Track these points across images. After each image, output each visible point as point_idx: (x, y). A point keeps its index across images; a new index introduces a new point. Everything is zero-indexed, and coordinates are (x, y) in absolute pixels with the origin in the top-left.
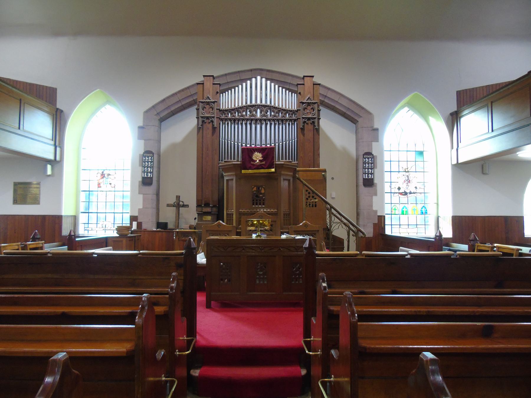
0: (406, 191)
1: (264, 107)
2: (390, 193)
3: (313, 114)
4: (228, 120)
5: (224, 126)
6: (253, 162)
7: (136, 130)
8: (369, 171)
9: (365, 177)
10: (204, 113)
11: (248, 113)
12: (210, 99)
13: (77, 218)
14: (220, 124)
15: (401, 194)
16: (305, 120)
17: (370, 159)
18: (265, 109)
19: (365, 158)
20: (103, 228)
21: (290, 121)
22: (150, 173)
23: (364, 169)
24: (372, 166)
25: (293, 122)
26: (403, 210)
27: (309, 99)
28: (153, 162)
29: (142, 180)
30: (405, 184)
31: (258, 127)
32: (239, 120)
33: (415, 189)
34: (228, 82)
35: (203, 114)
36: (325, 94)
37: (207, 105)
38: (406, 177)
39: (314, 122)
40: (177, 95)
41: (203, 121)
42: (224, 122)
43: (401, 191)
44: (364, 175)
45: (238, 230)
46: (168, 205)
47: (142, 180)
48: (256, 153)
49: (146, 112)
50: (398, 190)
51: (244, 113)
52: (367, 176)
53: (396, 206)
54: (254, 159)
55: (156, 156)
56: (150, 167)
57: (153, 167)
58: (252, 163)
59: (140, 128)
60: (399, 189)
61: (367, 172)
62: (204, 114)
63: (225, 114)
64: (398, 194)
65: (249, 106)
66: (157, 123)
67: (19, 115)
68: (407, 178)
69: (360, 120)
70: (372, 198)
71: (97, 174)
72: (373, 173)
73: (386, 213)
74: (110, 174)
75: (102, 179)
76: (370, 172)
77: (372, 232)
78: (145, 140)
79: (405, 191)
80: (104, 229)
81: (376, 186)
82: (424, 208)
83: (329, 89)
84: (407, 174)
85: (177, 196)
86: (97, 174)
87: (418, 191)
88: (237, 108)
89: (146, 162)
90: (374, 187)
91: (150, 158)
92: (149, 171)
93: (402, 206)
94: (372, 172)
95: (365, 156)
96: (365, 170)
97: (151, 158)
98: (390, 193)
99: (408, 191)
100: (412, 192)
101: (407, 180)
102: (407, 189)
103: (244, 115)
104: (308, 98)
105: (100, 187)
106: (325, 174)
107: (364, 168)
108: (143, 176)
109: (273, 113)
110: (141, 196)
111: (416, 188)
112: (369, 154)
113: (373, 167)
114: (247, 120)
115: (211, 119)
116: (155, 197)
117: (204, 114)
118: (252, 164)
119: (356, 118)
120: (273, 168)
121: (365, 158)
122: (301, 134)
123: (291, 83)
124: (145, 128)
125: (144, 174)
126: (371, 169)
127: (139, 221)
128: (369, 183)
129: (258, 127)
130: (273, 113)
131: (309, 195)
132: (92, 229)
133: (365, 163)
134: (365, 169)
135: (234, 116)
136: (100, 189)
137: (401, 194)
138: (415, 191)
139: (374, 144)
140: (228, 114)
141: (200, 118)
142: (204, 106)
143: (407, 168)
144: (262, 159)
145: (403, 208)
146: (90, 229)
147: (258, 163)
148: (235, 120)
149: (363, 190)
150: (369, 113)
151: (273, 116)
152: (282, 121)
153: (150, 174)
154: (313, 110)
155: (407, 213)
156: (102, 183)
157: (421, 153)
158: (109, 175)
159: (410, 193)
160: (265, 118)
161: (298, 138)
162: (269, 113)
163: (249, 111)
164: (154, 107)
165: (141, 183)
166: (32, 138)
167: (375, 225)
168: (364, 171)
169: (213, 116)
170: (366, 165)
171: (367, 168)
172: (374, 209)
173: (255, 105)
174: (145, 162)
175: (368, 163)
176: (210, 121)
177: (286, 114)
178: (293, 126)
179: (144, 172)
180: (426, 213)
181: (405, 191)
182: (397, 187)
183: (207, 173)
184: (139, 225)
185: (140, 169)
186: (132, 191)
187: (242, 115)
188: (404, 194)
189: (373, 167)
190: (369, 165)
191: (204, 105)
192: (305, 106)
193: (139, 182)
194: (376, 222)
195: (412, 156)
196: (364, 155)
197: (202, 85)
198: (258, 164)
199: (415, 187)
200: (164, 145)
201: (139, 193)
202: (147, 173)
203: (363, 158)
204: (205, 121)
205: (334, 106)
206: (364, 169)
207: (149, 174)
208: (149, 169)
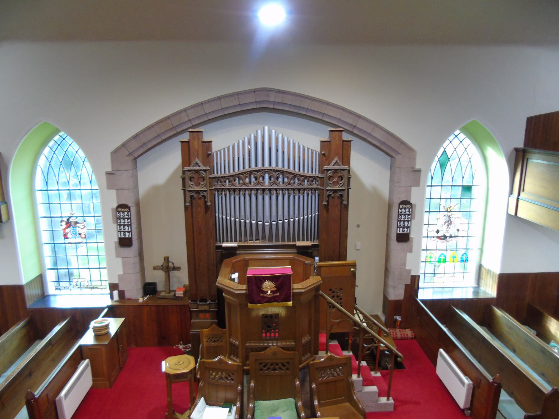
0: (446, 234)
1: (274, 173)
3: (341, 184)
4: (226, 190)
5: (220, 197)
6: (262, 293)
7: (104, 177)
8: (405, 224)
9: (400, 231)
10: (192, 185)
11: (253, 180)
12: (199, 166)
13: (43, 276)
14: (215, 195)
15: (439, 238)
16: (330, 193)
17: (407, 210)
18: (275, 175)
19: (401, 209)
20: (77, 287)
21: (309, 190)
22: (128, 232)
23: (399, 222)
24: (409, 218)
25: (313, 192)
26: (440, 257)
27: (336, 164)
28: (130, 218)
30: (445, 226)
31: (267, 198)
32: (240, 190)
33: (457, 231)
34: (223, 108)
35: (190, 187)
36: (354, 124)
37: (196, 173)
38: (447, 217)
39: (341, 196)
40: (154, 127)
41: (192, 197)
42: (220, 192)
43: (439, 235)
44: (398, 229)
45: (245, 368)
46: (155, 268)
47: (118, 240)
48: (267, 282)
49: (115, 153)
50: (436, 233)
51: (247, 180)
52: (403, 230)
53: (432, 253)
54: (264, 290)
55: (133, 210)
56: (128, 225)
57: (131, 225)
58: (262, 295)
59: (108, 173)
60: (438, 232)
62: (192, 186)
63: (221, 182)
64: (435, 238)
65: (253, 171)
66: (130, 165)
68: (448, 218)
69: (398, 157)
70: (406, 256)
71: (61, 222)
72: (409, 227)
73: (420, 273)
74: (78, 221)
75: (69, 229)
76: (406, 225)
77: (403, 294)
78: (116, 189)
79: (444, 234)
80: (79, 288)
81: (412, 242)
82: (465, 255)
83: (360, 117)
84: (449, 214)
85: (165, 258)
86: (61, 222)
87: (460, 234)
88: (238, 173)
89: (122, 219)
90: (409, 243)
91: (407, 210)
92: (127, 230)
93: (439, 253)
94: (409, 226)
95: (401, 206)
97: (128, 213)
99: (448, 235)
100: (453, 236)
101: (448, 221)
102: (447, 232)
103: (247, 183)
104: (335, 162)
105: (67, 238)
106: (354, 270)
107: (399, 221)
108: (120, 236)
109: (286, 180)
110: (120, 260)
111: (458, 230)
112: (406, 203)
113: (410, 219)
114: (251, 190)
115: (203, 193)
116: (137, 260)
117: (192, 186)
118: (262, 296)
119: (393, 154)
120: (291, 301)
121: (401, 209)
122: (324, 210)
123: (309, 108)
124: (116, 174)
125: (120, 233)
126: (408, 221)
127: (120, 289)
128: (404, 238)
129: (267, 198)
130: (286, 180)
131: (336, 296)
132: (64, 288)
133: (400, 214)
134: (401, 221)
135: (233, 185)
136: (67, 241)
137: (439, 238)
138: (456, 235)
139: (414, 189)
140: (225, 182)
141: (187, 193)
142: (191, 175)
143: (449, 207)
144: (275, 289)
145: (441, 256)
146: (62, 288)
147: (269, 295)
148: (234, 190)
149: (395, 245)
150: (410, 149)
151: (287, 184)
152: (299, 190)
153: (128, 234)
154: (340, 178)
155: (445, 261)
156: (70, 233)
157: (467, 189)
158: (77, 223)
159: (451, 237)
160: (276, 187)
161: (320, 212)
162: (280, 180)
163: (253, 178)
164: (123, 145)
165: (118, 244)
167: (407, 286)
168: (399, 224)
169: (205, 189)
170: (401, 217)
171: (402, 221)
172: (408, 268)
173: (262, 170)
174: (120, 219)
175: (405, 215)
176: (200, 196)
177: (303, 181)
178: (313, 197)
179: (121, 232)
180: (466, 260)
181: (444, 234)
182: (436, 230)
183: (202, 263)
184: (122, 294)
185: (114, 228)
186: (108, 254)
187: (244, 183)
188: (443, 238)
189: (410, 219)
190: (405, 217)
191: (191, 174)
192: (331, 173)
193: (115, 242)
194: (409, 282)
195: (458, 192)
196: (400, 204)
197: (187, 143)
198: (270, 296)
199: (457, 229)
200: (143, 189)
201: (117, 256)
202: (125, 232)
203: (399, 208)
204: (194, 197)
205: (366, 138)
206: (399, 222)
207: (127, 234)
208: (126, 228)
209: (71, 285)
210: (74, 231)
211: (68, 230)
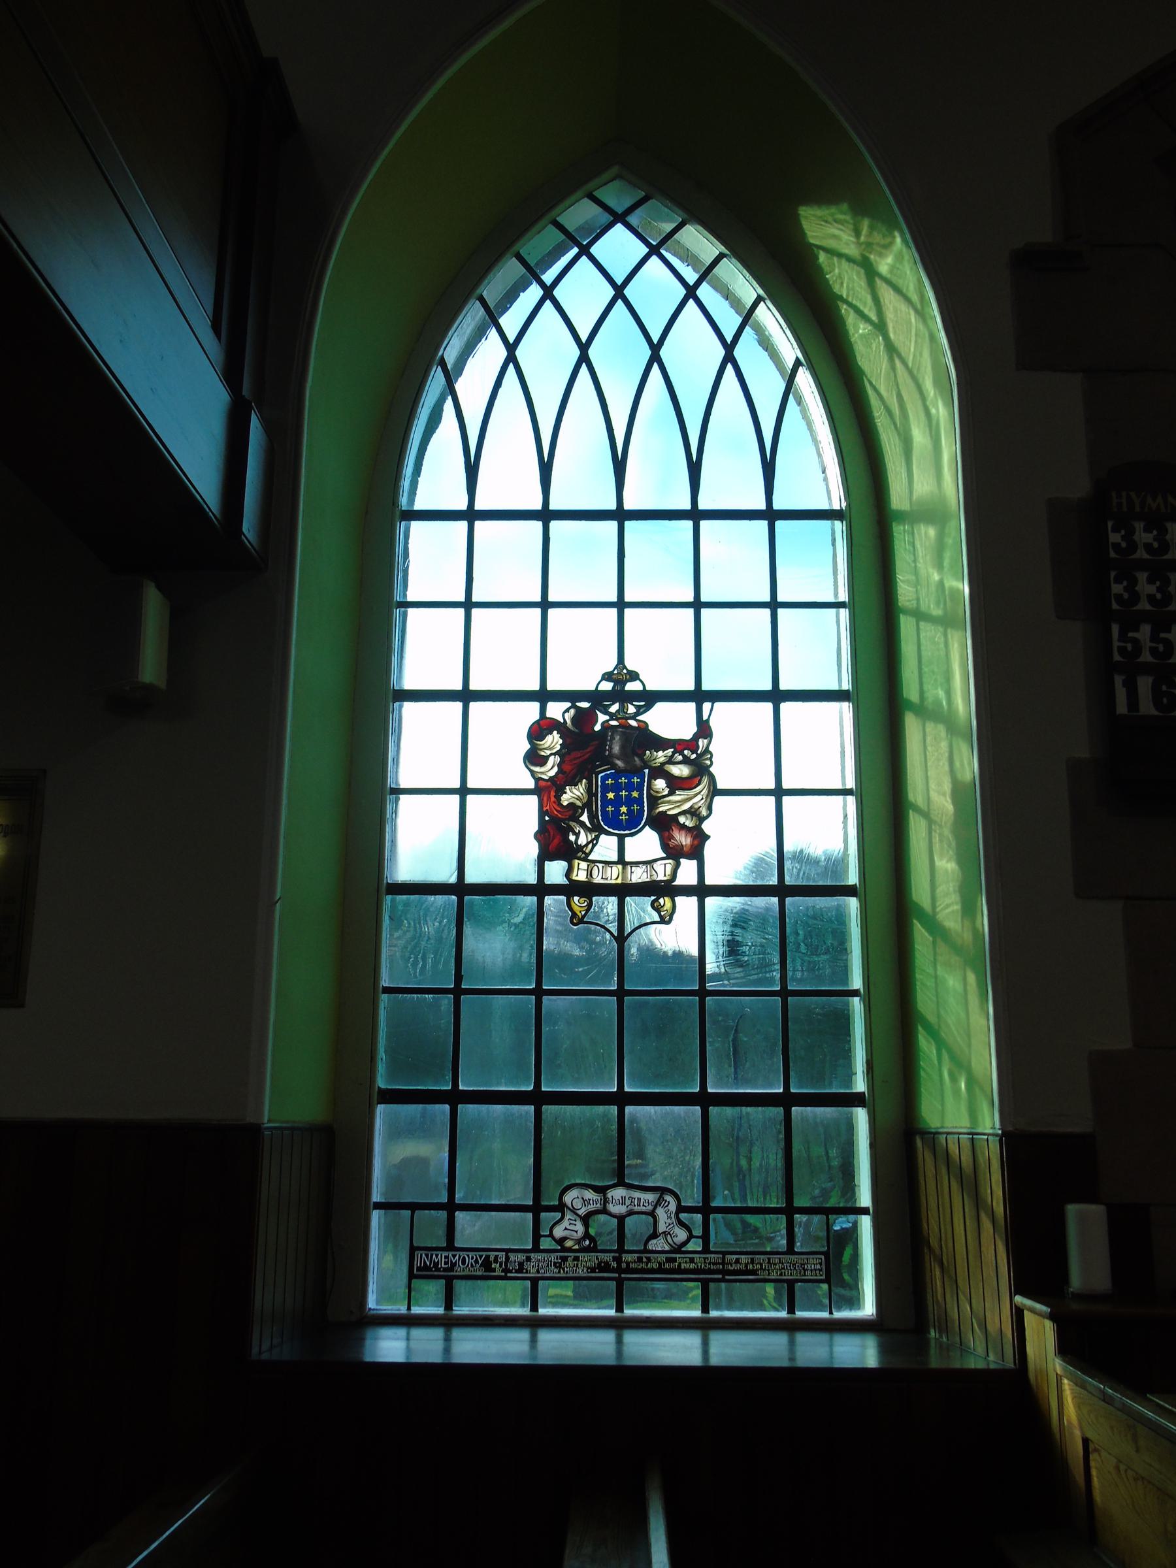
2: (459, 978)
9: (1133, 703)
20: (589, 1259)
23: (1115, 629)
29: (672, 775)
44: (1118, 680)
61: (1146, 657)
67: (126, 220)
96: (1123, 637)
98: (459, 978)
136: (687, 873)
166: (841, 734)
168: (1116, 644)
209: (546, 1244)
210: (617, 802)
211: (572, 795)
